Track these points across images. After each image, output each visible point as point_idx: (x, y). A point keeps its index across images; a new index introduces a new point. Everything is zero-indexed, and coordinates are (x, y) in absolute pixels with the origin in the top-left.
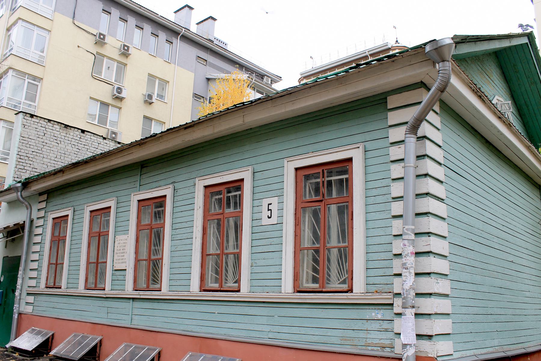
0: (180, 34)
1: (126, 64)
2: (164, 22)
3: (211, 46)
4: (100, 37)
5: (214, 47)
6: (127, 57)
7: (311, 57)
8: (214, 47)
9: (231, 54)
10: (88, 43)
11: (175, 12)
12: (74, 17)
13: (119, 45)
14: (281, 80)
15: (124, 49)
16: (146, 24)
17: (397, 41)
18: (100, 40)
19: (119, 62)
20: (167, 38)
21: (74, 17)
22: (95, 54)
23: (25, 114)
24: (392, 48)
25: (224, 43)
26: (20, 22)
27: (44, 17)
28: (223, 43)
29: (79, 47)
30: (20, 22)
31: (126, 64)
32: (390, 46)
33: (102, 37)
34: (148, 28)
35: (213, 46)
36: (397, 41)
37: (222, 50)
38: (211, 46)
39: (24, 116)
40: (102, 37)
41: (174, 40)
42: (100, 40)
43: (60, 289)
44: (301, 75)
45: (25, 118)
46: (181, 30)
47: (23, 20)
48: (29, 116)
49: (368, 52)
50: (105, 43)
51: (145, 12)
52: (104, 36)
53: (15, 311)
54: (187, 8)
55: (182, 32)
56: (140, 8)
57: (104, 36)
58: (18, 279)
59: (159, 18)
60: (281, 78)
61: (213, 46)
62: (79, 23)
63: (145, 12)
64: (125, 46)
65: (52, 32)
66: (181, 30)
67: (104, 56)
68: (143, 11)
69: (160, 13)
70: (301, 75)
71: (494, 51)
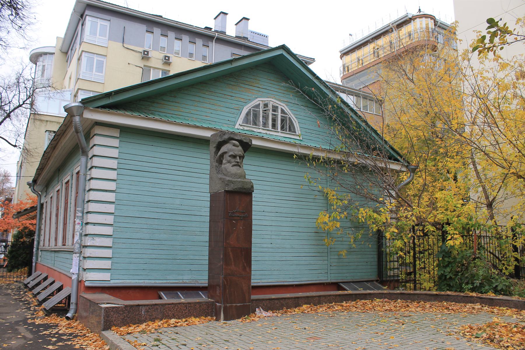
0: (214, 38)
1: (170, 71)
2: (199, 31)
3: (244, 43)
4: (144, 54)
5: (246, 43)
6: (169, 65)
7: (350, 35)
8: (246, 43)
9: (263, 47)
10: (137, 59)
11: (215, 19)
12: (123, 41)
13: (161, 56)
14: (314, 61)
15: (165, 59)
16: (185, 35)
17: (420, 10)
18: (145, 55)
19: (163, 70)
20: (203, 43)
21: (123, 41)
22: (143, 67)
23: (49, 132)
24: (413, 18)
25: (264, 36)
26: (84, 54)
27: (100, 47)
28: (263, 36)
29: (129, 64)
30: (84, 54)
31: (170, 71)
32: (410, 16)
33: (146, 53)
34: (186, 38)
35: (245, 43)
36: (420, 10)
37: (254, 44)
38: (244, 43)
39: (49, 133)
40: (146, 53)
41: (210, 44)
42: (145, 55)
43: (65, 246)
44: (341, 52)
45: (50, 134)
46: (215, 35)
47: (85, 51)
48: (53, 132)
49: (392, 24)
50: (149, 58)
51: (182, 26)
52: (148, 52)
53: (33, 261)
54: (222, 14)
55: (215, 36)
56: (177, 24)
57: (148, 52)
58: (35, 241)
59: (194, 28)
60: (314, 59)
61: (245, 43)
62: (127, 45)
63: (182, 26)
64: (166, 56)
65: (108, 56)
66: (215, 35)
67: (151, 67)
68: (180, 26)
69: (195, 24)
70: (341, 52)
71: (96, 121)
